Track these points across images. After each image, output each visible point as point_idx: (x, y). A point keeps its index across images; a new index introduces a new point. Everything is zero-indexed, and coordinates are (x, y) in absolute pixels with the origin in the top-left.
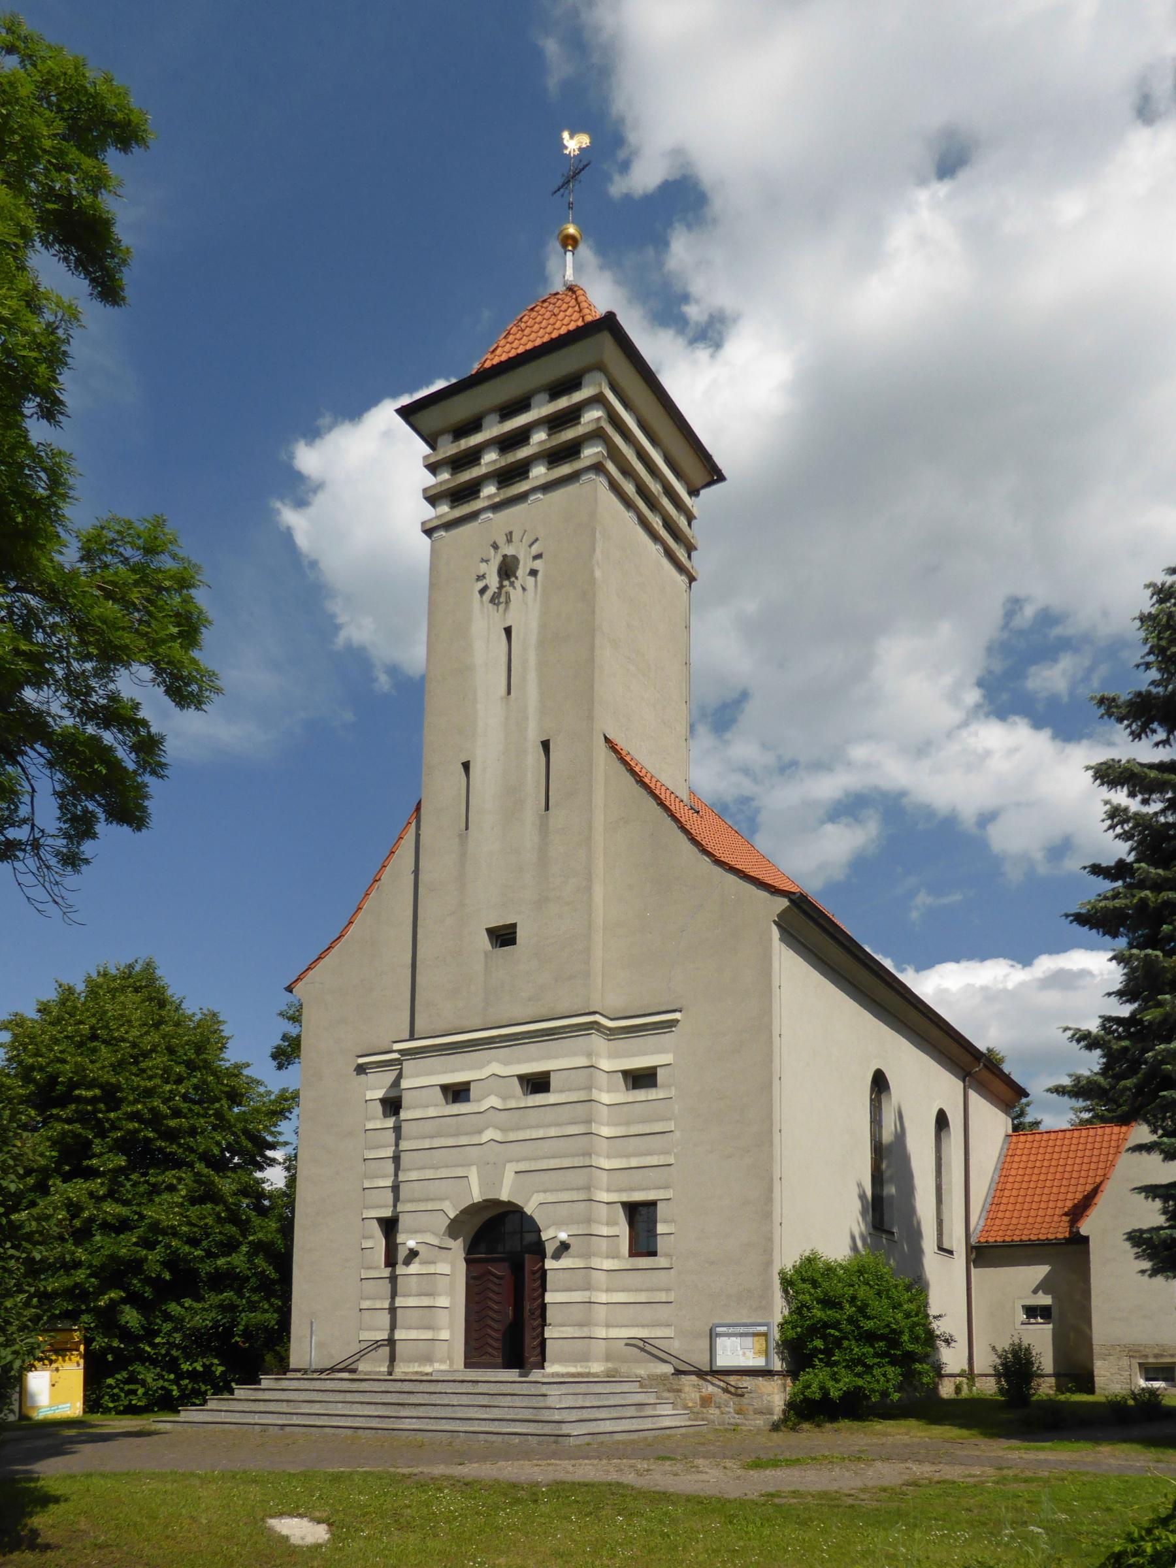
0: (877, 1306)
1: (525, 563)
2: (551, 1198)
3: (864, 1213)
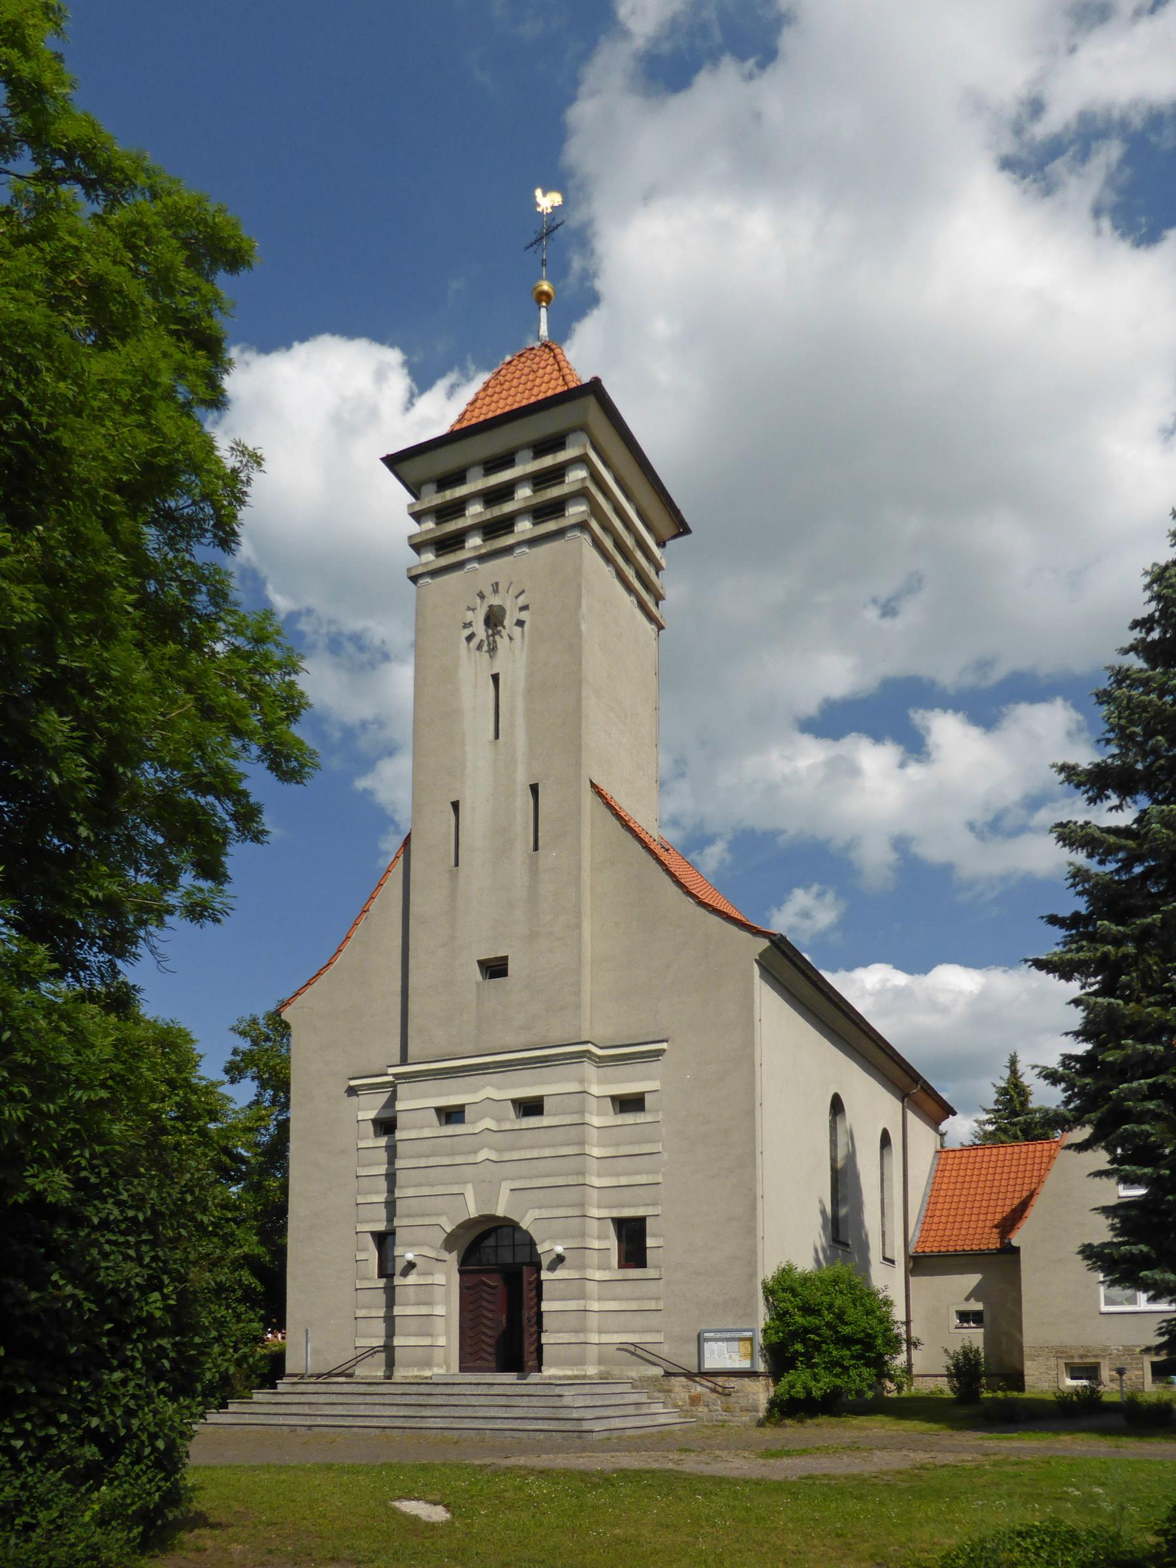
0: (851, 1314)
2: (545, 1213)
3: (824, 1227)
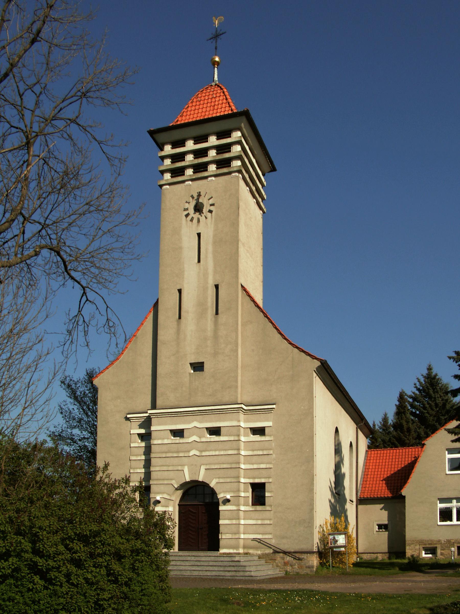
1: (207, 207)
2: (221, 480)
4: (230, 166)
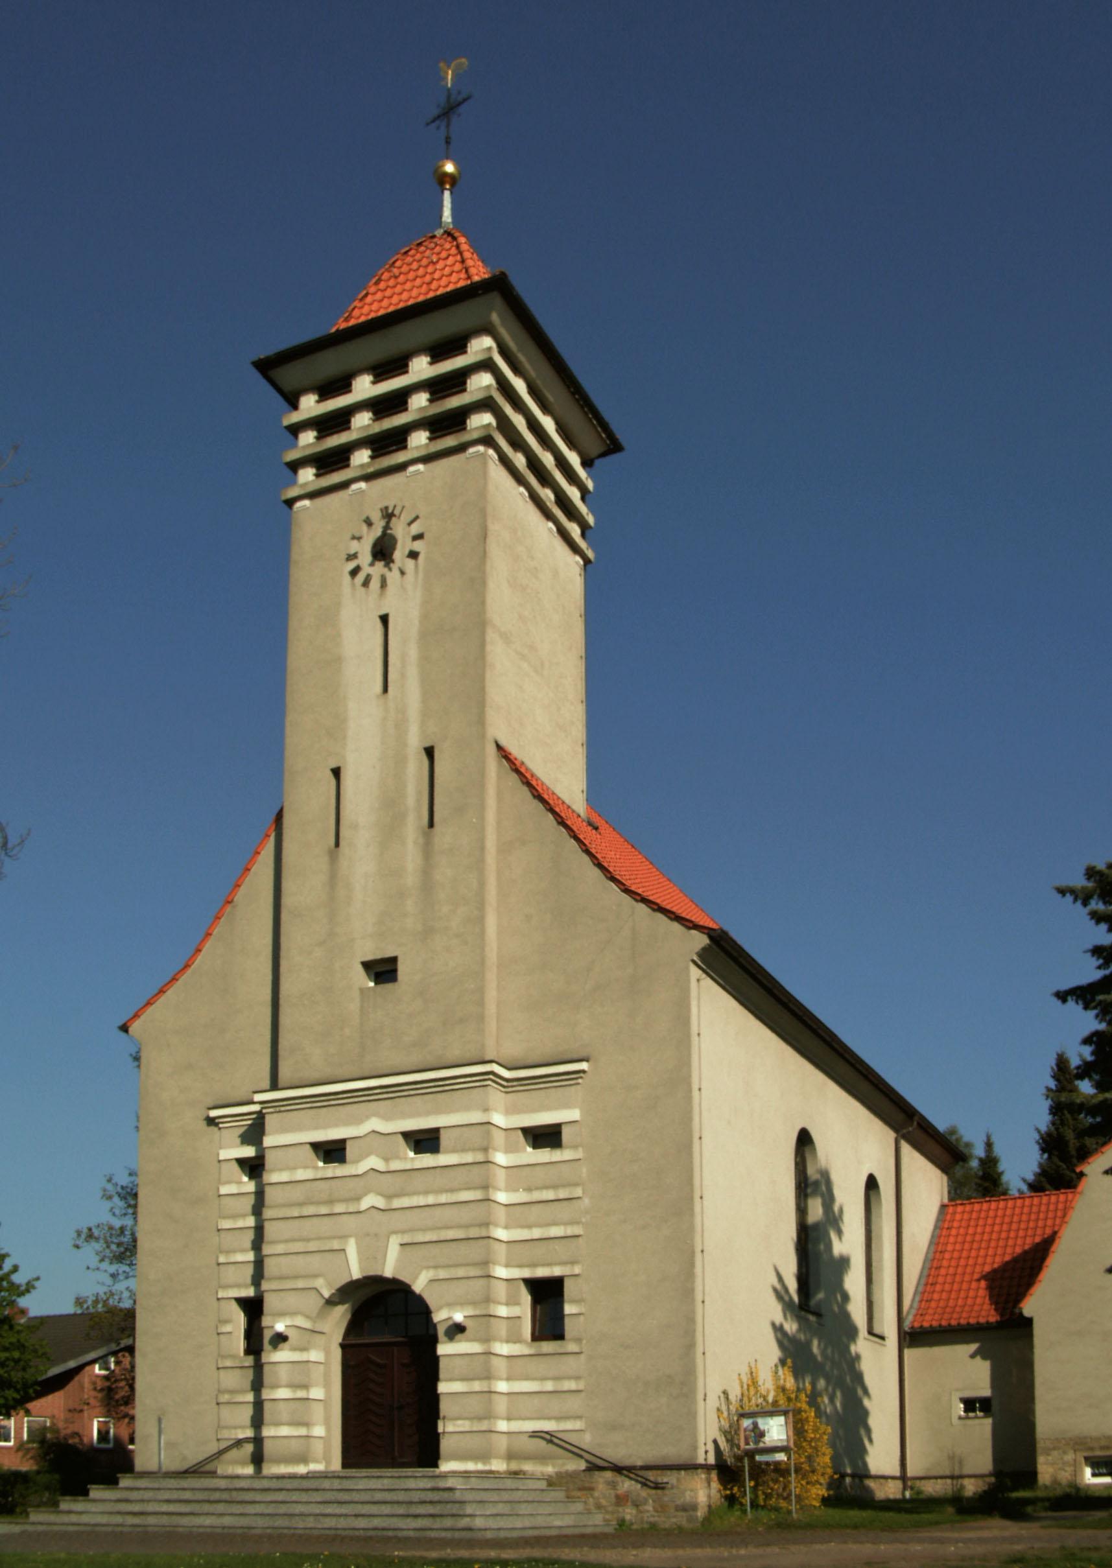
1: (404, 546)
2: (442, 1274)
4: (465, 429)
